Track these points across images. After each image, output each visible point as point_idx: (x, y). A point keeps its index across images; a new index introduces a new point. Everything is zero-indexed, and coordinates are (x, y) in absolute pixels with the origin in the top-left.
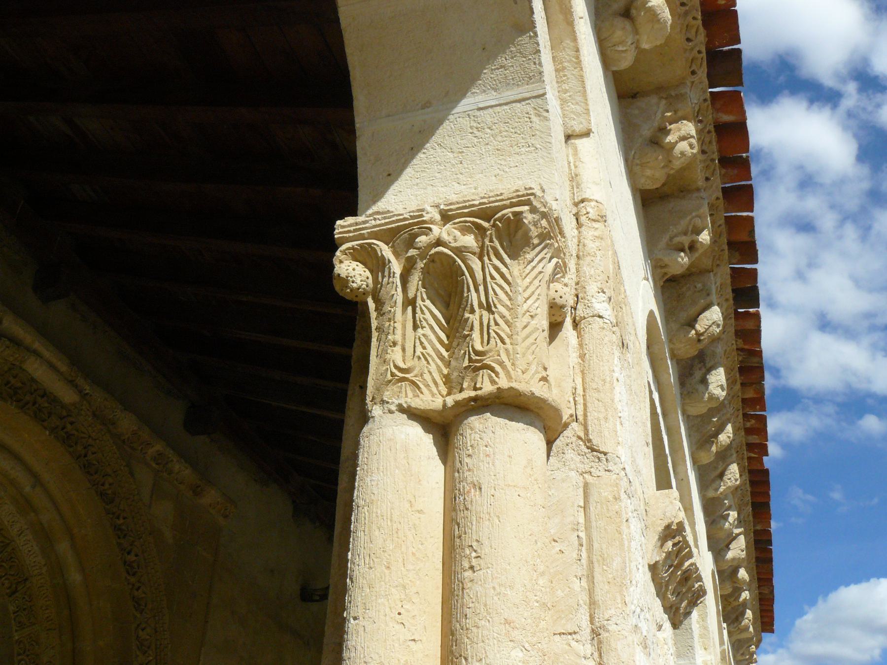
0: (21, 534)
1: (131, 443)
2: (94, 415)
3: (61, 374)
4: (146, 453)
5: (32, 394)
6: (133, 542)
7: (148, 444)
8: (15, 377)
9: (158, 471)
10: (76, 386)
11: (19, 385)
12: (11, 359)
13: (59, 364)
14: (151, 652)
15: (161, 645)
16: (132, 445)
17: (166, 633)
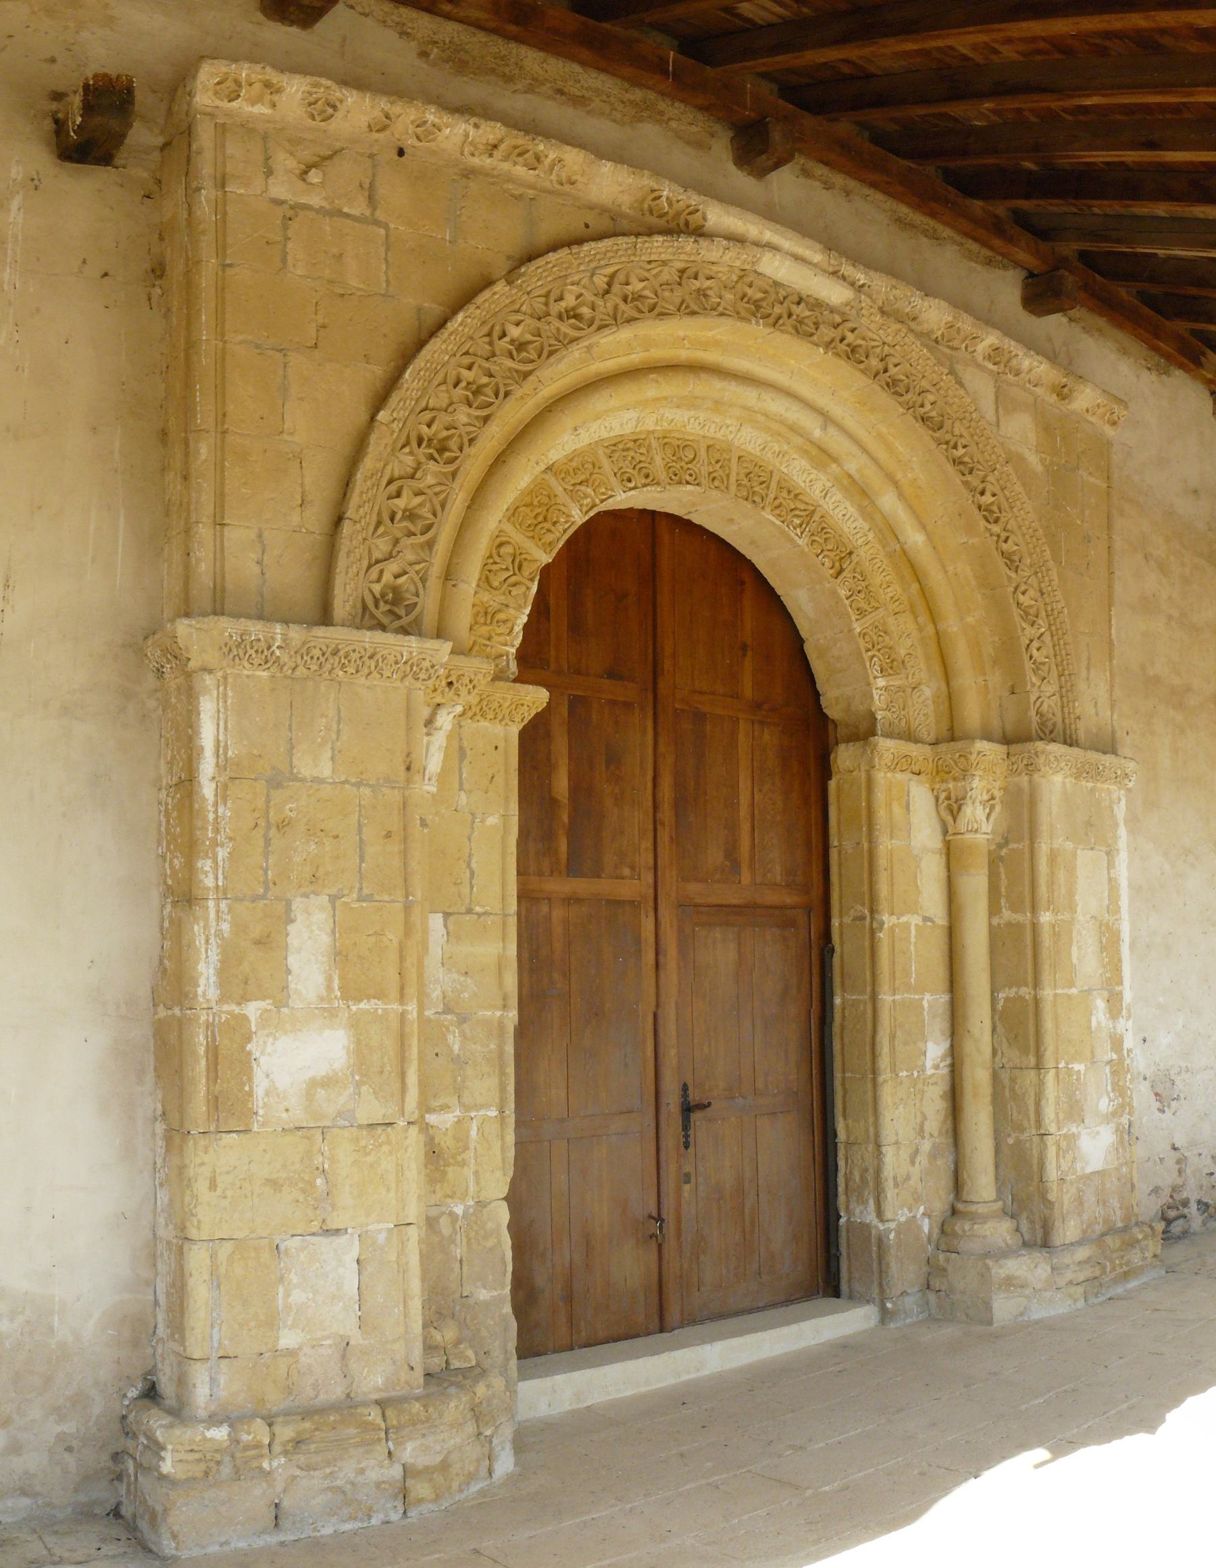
0: (826, 494)
1: (948, 341)
2: (883, 312)
3: (815, 265)
4: (975, 351)
5: (782, 303)
6: (986, 476)
7: (974, 338)
8: (750, 286)
9: (999, 373)
10: (844, 278)
11: (760, 295)
12: (738, 263)
13: (807, 254)
14: (1041, 622)
15: (1052, 610)
16: (951, 344)
17: (1056, 593)
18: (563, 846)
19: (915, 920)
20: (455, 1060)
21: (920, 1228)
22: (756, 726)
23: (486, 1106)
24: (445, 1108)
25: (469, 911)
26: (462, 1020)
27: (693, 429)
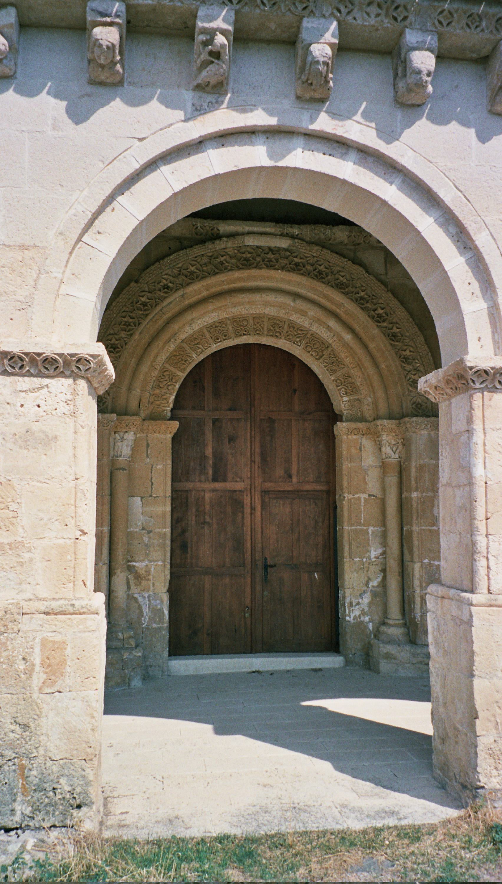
13: (268, 230)
14: (417, 361)
18: (210, 472)
19: (363, 496)
20: (146, 545)
21: (367, 627)
22: (301, 422)
23: (158, 561)
24: (143, 561)
25: (151, 496)
26: (149, 532)
27: (244, 312)
